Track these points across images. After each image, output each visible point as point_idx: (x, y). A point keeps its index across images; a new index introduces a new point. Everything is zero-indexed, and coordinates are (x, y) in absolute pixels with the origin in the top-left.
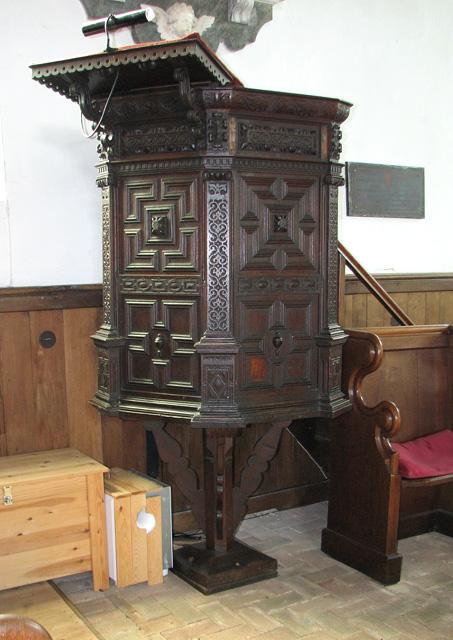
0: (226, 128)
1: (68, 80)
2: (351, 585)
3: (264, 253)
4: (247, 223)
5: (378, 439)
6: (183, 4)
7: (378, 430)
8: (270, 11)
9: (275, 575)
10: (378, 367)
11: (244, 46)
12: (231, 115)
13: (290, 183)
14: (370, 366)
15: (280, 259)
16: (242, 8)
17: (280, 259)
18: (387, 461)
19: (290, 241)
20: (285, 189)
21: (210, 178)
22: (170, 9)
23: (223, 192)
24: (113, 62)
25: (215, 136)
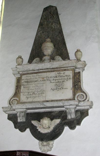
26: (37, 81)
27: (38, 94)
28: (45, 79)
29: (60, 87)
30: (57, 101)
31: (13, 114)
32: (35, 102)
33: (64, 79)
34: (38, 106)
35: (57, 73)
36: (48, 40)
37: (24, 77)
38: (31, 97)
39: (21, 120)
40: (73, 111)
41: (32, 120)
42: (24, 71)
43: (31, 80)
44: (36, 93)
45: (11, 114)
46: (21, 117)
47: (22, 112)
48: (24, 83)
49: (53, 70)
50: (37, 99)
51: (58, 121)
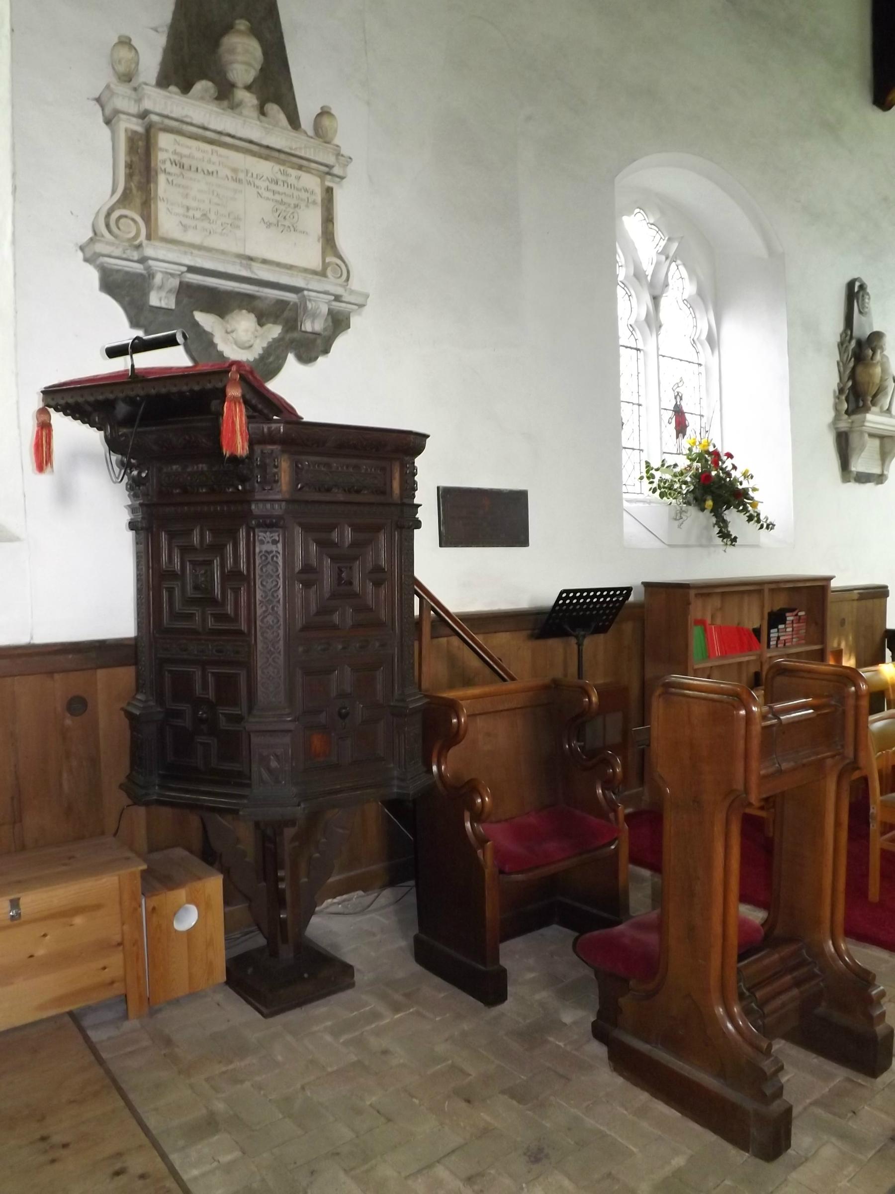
0: (276, 467)
1: (89, 409)
2: (442, 995)
3: (323, 611)
4: (304, 576)
5: (468, 825)
6: (244, 311)
7: (467, 815)
8: (348, 319)
9: (352, 985)
10: (461, 741)
11: (316, 358)
12: (283, 451)
13: (356, 528)
14: (454, 737)
15: (343, 616)
16: (314, 316)
17: (343, 616)
18: (479, 852)
19: (356, 595)
20: (348, 533)
21: (259, 525)
22: (228, 317)
23: (275, 542)
24: (139, 391)
25: (264, 477)
26: (215, 174)
27: (219, 223)
28: (241, 176)
29: (287, 223)
30: (290, 267)
31: (127, 273)
32: (209, 250)
33: (299, 198)
34: (221, 268)
35: (277, 167)
36: (242, 25)
37: (311, 182)
38: (196, 228)
39: (162, 302)
40: (324, 309)
41: (196, 310)
42: (167, 117)
43: (194, 164)
44: (212, 216)
45: (118, 271)
46: (166, 290)
47: (172, 275)
48: (168, 163)
49: (267, 152)
50: (215, 242)
51: (275, 331)
